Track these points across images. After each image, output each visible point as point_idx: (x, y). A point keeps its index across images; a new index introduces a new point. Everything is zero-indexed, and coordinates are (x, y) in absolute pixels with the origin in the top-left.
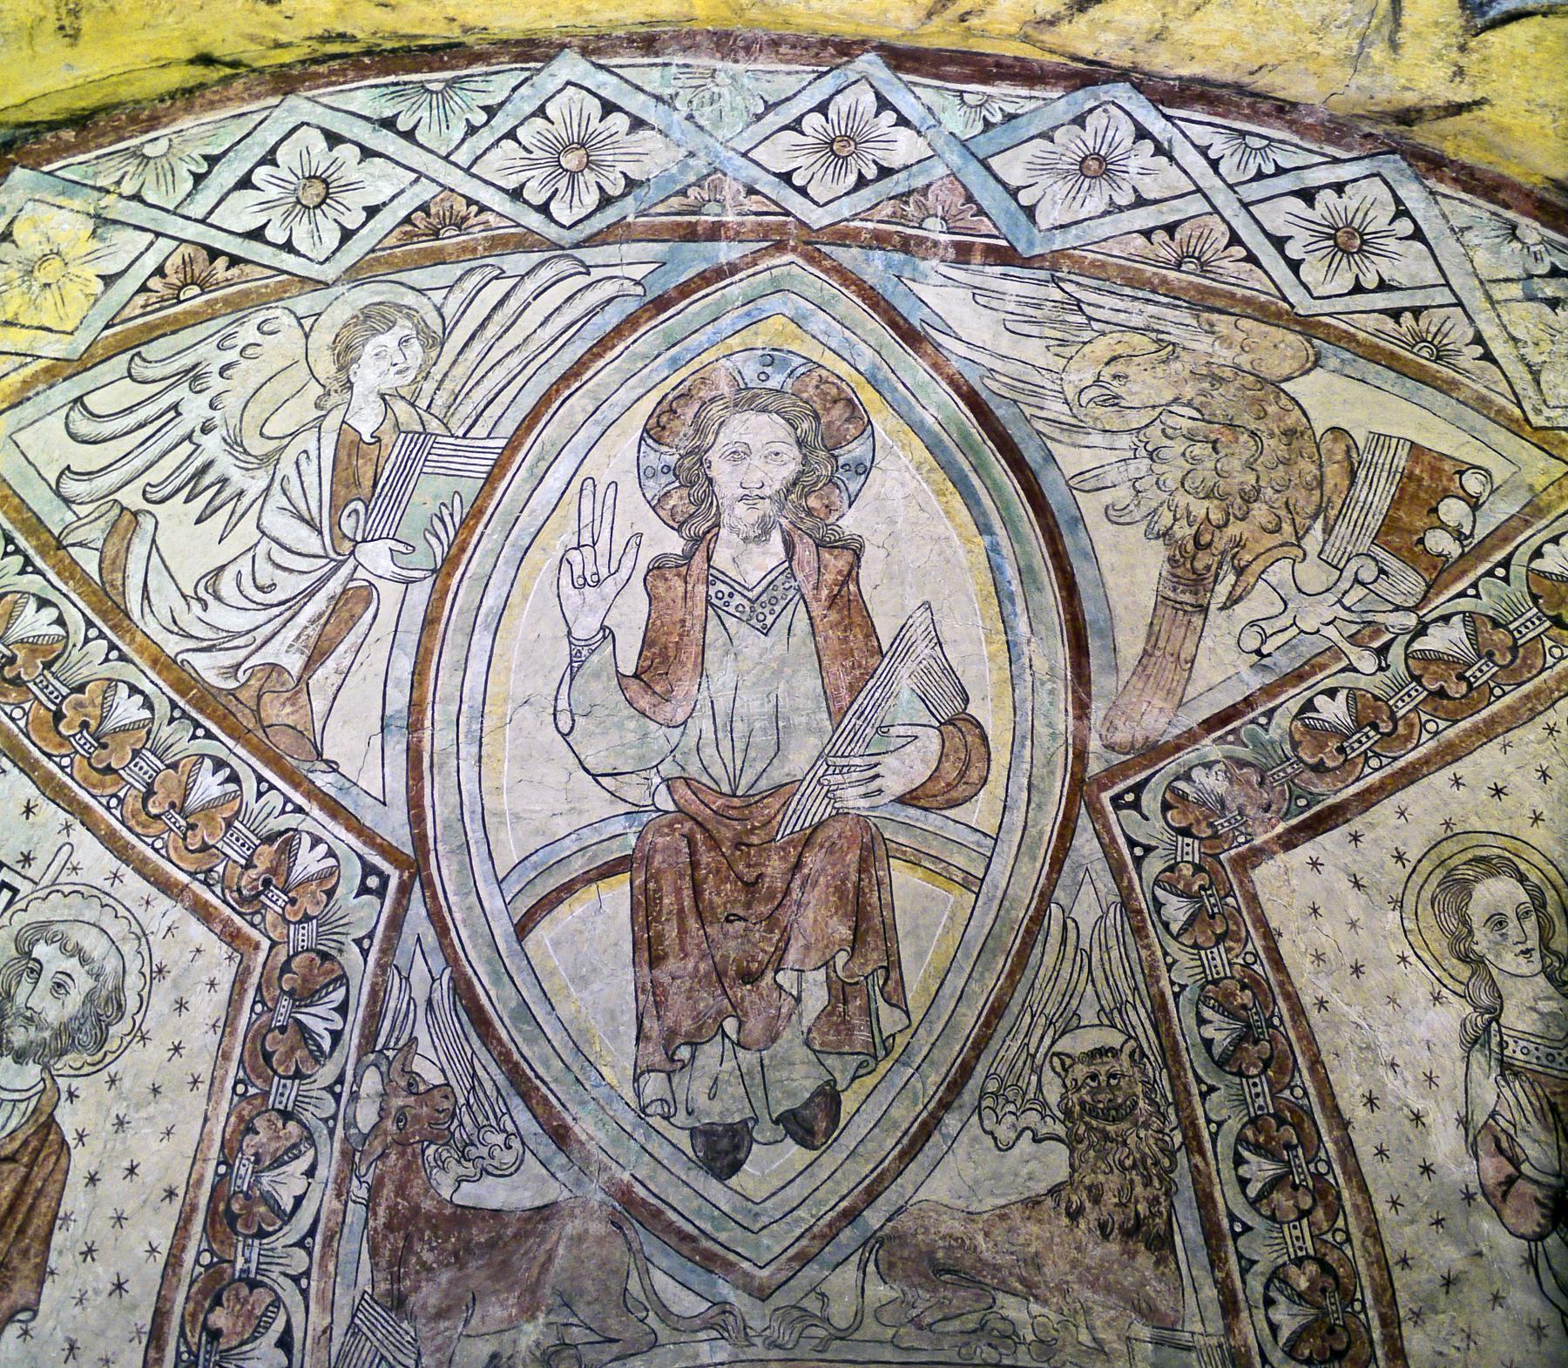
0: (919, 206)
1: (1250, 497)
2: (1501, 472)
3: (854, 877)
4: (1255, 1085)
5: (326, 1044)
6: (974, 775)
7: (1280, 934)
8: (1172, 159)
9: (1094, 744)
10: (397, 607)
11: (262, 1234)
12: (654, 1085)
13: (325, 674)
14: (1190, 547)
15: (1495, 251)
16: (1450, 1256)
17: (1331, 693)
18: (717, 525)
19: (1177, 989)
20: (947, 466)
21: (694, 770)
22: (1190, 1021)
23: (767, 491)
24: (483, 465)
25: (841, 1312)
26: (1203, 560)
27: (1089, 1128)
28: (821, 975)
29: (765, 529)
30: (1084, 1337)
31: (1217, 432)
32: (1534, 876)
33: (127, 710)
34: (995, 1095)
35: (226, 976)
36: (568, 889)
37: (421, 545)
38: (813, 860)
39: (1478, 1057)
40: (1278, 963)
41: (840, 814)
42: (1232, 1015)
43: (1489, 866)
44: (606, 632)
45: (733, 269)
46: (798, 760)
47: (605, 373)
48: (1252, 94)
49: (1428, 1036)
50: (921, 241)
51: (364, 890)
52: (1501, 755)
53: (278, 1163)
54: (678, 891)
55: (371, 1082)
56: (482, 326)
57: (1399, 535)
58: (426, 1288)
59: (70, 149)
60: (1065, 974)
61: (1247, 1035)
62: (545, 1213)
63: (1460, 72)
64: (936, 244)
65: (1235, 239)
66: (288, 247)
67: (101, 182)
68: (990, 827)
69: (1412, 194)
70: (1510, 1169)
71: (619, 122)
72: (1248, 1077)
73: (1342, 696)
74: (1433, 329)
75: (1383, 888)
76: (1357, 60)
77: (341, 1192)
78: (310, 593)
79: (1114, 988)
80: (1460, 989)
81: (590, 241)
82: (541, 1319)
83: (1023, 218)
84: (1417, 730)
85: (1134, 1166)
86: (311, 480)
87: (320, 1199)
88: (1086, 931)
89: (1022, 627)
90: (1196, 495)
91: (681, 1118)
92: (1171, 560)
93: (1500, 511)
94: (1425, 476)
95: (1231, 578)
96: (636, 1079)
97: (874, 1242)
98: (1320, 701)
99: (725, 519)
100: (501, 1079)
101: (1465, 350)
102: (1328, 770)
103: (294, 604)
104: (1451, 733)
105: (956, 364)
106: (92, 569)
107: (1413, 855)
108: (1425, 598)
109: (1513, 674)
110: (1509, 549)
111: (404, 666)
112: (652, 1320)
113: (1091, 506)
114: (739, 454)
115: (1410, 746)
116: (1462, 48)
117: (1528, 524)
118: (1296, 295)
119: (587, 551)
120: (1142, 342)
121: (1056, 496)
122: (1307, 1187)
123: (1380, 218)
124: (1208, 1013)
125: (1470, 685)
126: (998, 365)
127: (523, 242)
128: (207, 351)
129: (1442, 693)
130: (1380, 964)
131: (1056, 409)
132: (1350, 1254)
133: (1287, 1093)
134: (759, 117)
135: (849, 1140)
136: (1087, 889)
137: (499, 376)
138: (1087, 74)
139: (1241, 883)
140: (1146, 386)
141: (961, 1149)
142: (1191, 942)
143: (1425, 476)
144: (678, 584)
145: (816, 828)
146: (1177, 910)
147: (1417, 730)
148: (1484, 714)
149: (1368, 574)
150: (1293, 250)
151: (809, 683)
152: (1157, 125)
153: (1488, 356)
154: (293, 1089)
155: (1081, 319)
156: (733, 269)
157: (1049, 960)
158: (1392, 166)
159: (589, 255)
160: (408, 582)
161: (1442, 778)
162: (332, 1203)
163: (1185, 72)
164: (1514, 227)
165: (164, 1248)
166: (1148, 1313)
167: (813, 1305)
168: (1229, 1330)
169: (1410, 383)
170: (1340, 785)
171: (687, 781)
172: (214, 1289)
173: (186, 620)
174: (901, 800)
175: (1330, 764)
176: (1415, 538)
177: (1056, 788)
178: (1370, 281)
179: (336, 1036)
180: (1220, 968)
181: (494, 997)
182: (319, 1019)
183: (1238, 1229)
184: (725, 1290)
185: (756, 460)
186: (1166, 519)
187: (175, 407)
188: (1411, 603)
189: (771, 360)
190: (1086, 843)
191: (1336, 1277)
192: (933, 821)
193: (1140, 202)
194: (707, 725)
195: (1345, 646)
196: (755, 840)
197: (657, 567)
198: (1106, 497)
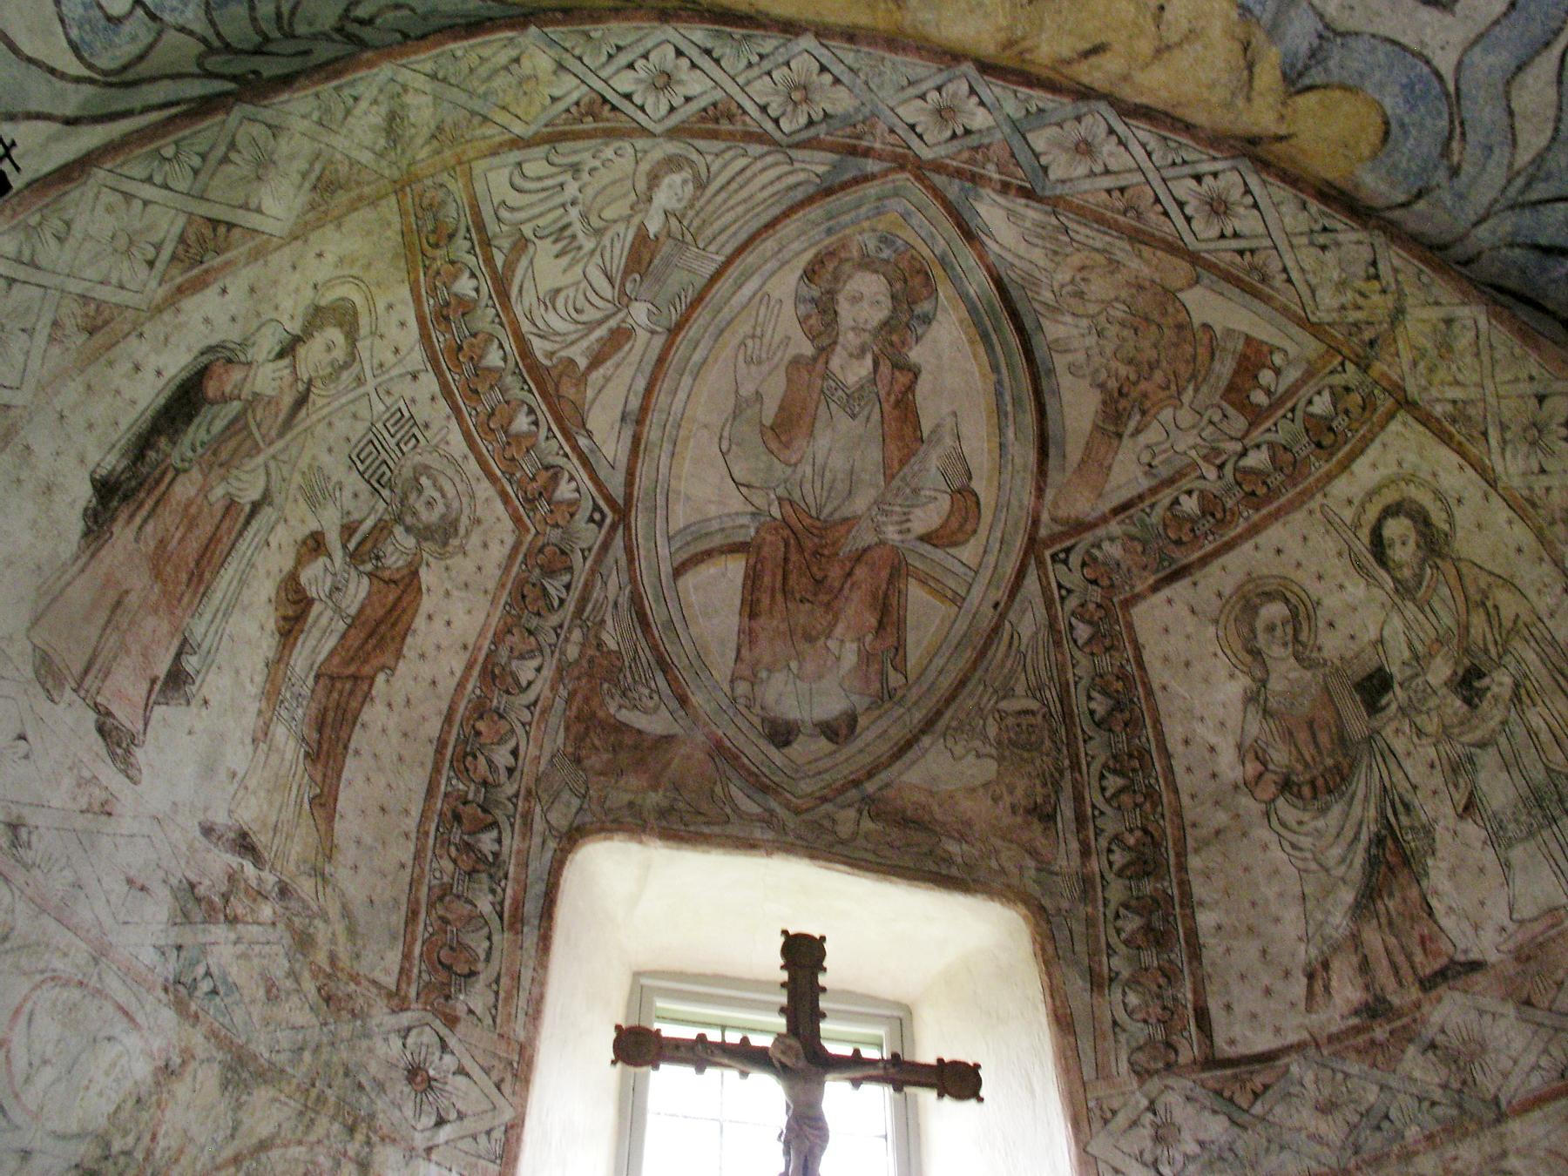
0: (985, 155)
1: (1153, 366)
3: (884, 587)
5: (556, 603)
6: (969, 527)
8: (1126, 148)
9: (1045, 517)
10: (643, 346)
11: (508, 692)
12: (742, 688)
13: (597, 376)
14: (1116, 395)
15: (1295, 217)
16: (1221, 818)
17: (1189, 493)
18: (835, 343)
20: (978, 324)
21: (796, 496)
22: (1083, 698)
23: (869, 327)
24: (712, 267)
25: (844, 830)
26: (1123, 403)
27: (1012, 753)
28: (855, 646)
29: (863, 350)
30: (994, 864)
31: (1138, 322)
32: (1293, 600)
33: (494, 358)
34: (955, 729)
35: (510, 540)
36: (708, 554)
37: (665, 311)
38: (861, 572)
39: (1251, 708)
40: (1140, 664)
41: (882, 543)
43: (1269, 596)
44: (759, 396)
45: (873, 177)
46: (860, 504)
47: (790, 227)
48: (1173, 118)
50: (982, 176)
51: (591, 520)
53: (522, 657)
54: (774, 575)
55: (577, 635)
56: (729, 183)
57: (1236, 394)
58: (594, 758)
59: (558, 23)
60: (1009, 664)
61: (1118, 707)
62: (668, 739)
63: (1282, 117)
64: (990, 179)
65: (1157, 200)
66: (642, 109)
67: (567, 45)
68: (973, 563)
69: (1254, 182)
71: (827, 78)
73: (1195, 495)
76: (1228, 106)
77: (553, 688)
78: (600, 323)
79: (1038, 677)
81: (798, 146)
82: (661, 792)
83: (1041, 173)
86: (617, 252)
87: (541, 687)
88: (1025, 640)
89: (1011, 435)
90: (1122, 361)
91: (757, 710)
92: (1104, 403)
93: (1292, 375)
95: (1138, 417)
96: (732, 681)
97: (868, 800)
98: (1184, 499)
99: (841, 339)
100: (653, 662)
103: (591, 326)
105: (992, 258)
106: (499, 264)
108: (1247, 433)
109: (1293, 480)
111: (641, 384)
112: (728, 811)
113: (1060, 362)
114: (856, 299)
116: (1284, 104)
118: (1188, 238)
119: (757, 341)
120: (1100, 259)
121: (1040, 353)
123: (1236, 194)
124: (1094, 694)
126: (1016, 262)
127: (761, 138)
128: (587, 156)
129: (1253, 493)
131: (1047, 296)
134: (903, 88)
135: (859, 743)
136: (1029, 614)
137: (730, 217)
138: (1085, 94)
140: (1099, 287)
141: (930, 757)
144: (806, 375)
145: (865, 550)
146: (1083, 632)
149: (1216, 418)
150: (1189, 210)
151: (875, 454)
152: (1120, 128)
153: (1289, 280)
154: (534, 622)
155: (1066, 239)
156: (873, 177)
157: (1000, 655)
158: (1244, 165)
159: (794, 153)
160: (653, 332)
161: (1248, 546)
162: (547, 692)
163: (1138, 101)
165: (458, 674)
166: (1033, 853)
167: (827, 823)
168: (1083, 864)
169: (1248, 297)
171: (791, 503)
172: (480, 710)
173: (536, 313)
174: (922, 539)
177: (1019, 541)
178: (1228, 231)
179: (562, 601)
181: (656, 614)
182: (554, 587)
184: (773, 804)
185: (865, 304)
186: (1103, 375)
187: (562, 185)
189: (885, 240)
190: (1031, 583)
192: (938, 554)
193: (1107, 172)
194: (809, 470)
196: (826, 552)
197: (796, 362)
198: (1070, 357)
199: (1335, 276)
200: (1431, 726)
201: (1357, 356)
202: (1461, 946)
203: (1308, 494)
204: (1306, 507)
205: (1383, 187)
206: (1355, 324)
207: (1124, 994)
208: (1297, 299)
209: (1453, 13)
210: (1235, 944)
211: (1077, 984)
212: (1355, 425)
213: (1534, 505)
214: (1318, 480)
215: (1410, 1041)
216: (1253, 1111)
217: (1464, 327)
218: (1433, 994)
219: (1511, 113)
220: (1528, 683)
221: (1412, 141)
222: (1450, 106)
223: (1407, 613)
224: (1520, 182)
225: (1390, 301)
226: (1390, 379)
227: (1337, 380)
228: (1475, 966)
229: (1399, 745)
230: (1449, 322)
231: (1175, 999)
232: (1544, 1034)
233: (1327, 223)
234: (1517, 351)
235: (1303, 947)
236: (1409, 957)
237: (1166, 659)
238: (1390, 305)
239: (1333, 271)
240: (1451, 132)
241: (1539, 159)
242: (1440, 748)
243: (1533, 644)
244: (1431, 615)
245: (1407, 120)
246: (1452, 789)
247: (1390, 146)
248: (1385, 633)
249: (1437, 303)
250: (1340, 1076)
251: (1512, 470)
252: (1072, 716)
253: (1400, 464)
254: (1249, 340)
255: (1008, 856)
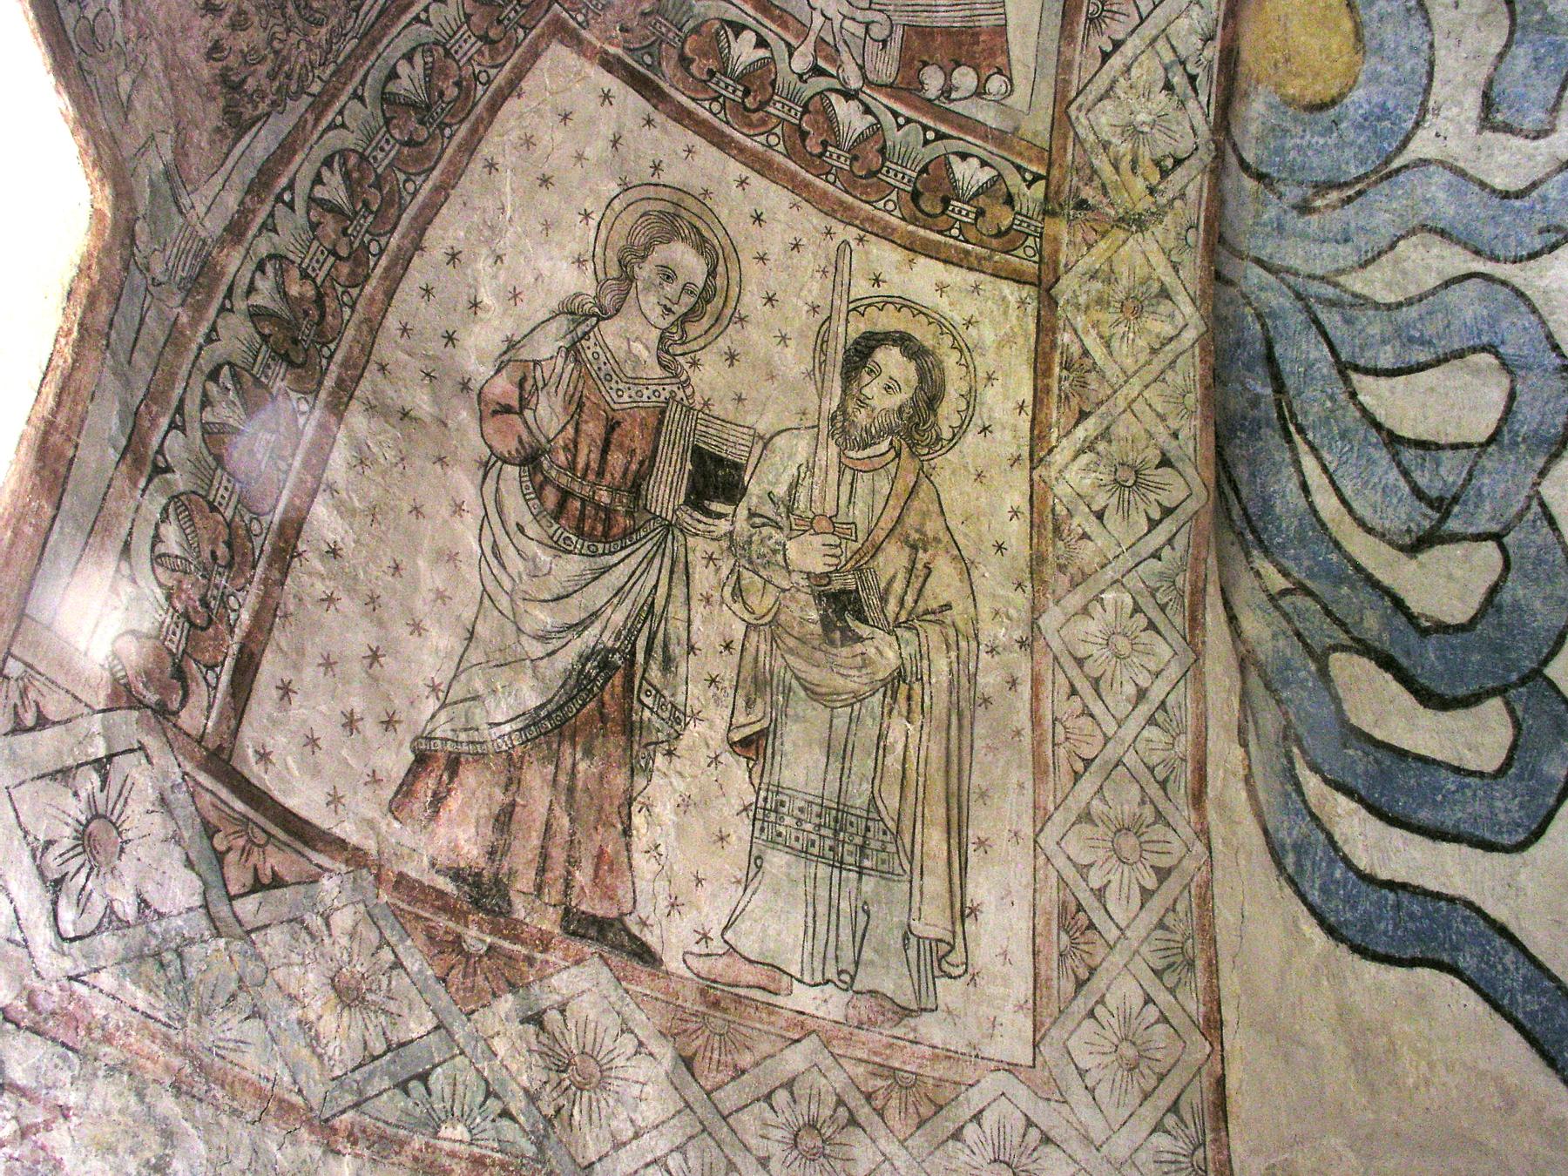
2: (1019, 99)
4: (387, 141)
7: (519, 96)
16: (421, 401)
17: (762, 43)
19: (423, 16)
22: (403, 45)
30: (125, 82)
32: (720, 282)
39: (563, 322)
40: (494, 107)
42: (429, 87)
43: (702, 245)
49: (546, 273)
52: (787, 204)
61: (424, 110)
70: (515, 403)
72: (388, 131)
73: (762, 53)
74: (1115, 8)
75: (626, 167)
80: (601, 276)
84: (762, 129)
85: (277, 53)
93: (986, 115)
94: (982, 46)
98: (749, 37)
101: (1105, 38)
102: (687, 69)
104: (780, 159)
107: (665, 178)
110: (954, 133)
115: (745, 130)
117: (985, 138)
122: (351, 243)
124: (418, 59)
125: (821, 155)
129: (804, 135)
130: (569, 199)
132: (346, 317)
133: (402, 177)
139: (541, 36)
142: (468, 11)
143: (982, 46)
147: (762, 129)
148: (809, 177)
149: (876, 31)
153: (1106, 57)
161: (736, 169)
164: (1212, 38)
168: (221, 242)
170: (680, 86)
175: (694, 68)
176: (925, 58)
180: (461, 53)
183: (287, 197)
188: (871, 76)
191: (323, 316)
195: (812, 38)
199: (1142, 117)
200: (762, 603)
201: (1058, 193)
202: (643, 910)
203: (847, 216)
204: (833, 223)
205: (1254, 128)
206: (1094, 171)
207: (165, 516)
208: (1086, 77)
209: (1479, 132)
210: (345, 603)
211: (107, 421)
212: (972, 234)
213: (1057, 530)
214: (872, 220)
215: (513, 987)
216: (237, 904)
217: (1172, 316)
218: (576, 945)
219: (1392, 246)
220: (917, 686)
221: (1322, 141)
222: (1375, 171)
223: (821, 453)
224: (1330, 292)
225: (1145, 203)
226: (1057, 251)
227: (1014, 181)
228: (645, 955)
229: (703, 578)
230: (1165, 294)
231: (224, 603)
232: (687, 1124)
233: (1201, 80)
234: (1191, 400)
235: (431, 705)
236: (573, 862)
237: (528, 142)
238: (1140, 207)
239: (1138, 109)
240: (1347, 184)
241: (1362, 302)
242: (753, 636)
243: (953, 654)
244: (845, 489)
245: (1343, 125)
246: (741, 703)
247: (1306, 116)
248: (779, 441)
249: (1175, 267)
250: (386, 956)
251: (1072, 475)
252: (373, 45)
253: (969, 323)
254: (1002, 30)
255: (149, 105)
